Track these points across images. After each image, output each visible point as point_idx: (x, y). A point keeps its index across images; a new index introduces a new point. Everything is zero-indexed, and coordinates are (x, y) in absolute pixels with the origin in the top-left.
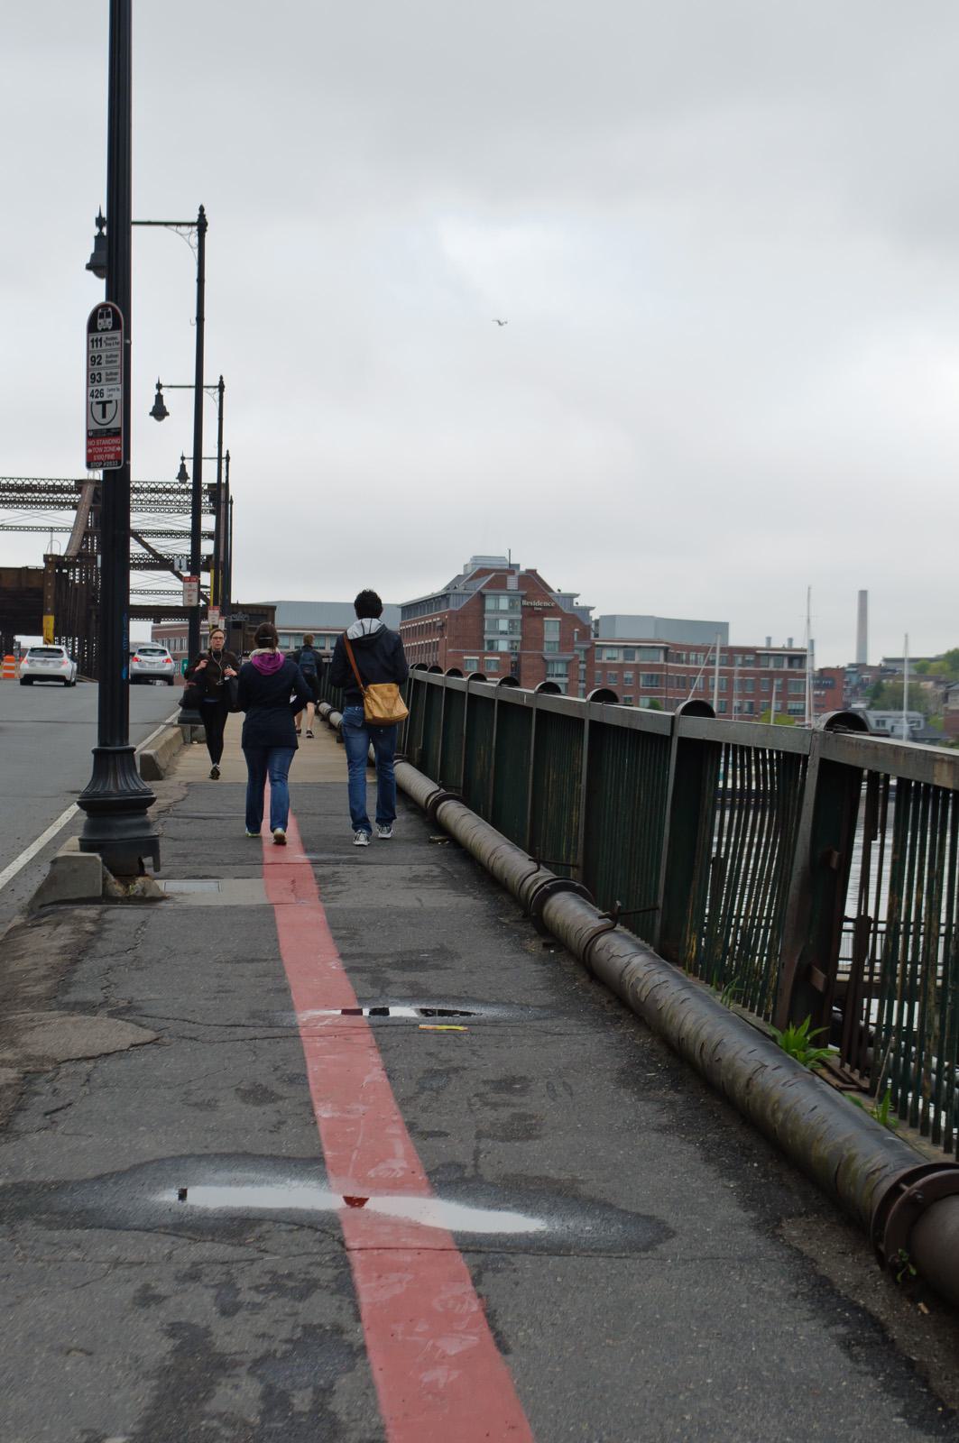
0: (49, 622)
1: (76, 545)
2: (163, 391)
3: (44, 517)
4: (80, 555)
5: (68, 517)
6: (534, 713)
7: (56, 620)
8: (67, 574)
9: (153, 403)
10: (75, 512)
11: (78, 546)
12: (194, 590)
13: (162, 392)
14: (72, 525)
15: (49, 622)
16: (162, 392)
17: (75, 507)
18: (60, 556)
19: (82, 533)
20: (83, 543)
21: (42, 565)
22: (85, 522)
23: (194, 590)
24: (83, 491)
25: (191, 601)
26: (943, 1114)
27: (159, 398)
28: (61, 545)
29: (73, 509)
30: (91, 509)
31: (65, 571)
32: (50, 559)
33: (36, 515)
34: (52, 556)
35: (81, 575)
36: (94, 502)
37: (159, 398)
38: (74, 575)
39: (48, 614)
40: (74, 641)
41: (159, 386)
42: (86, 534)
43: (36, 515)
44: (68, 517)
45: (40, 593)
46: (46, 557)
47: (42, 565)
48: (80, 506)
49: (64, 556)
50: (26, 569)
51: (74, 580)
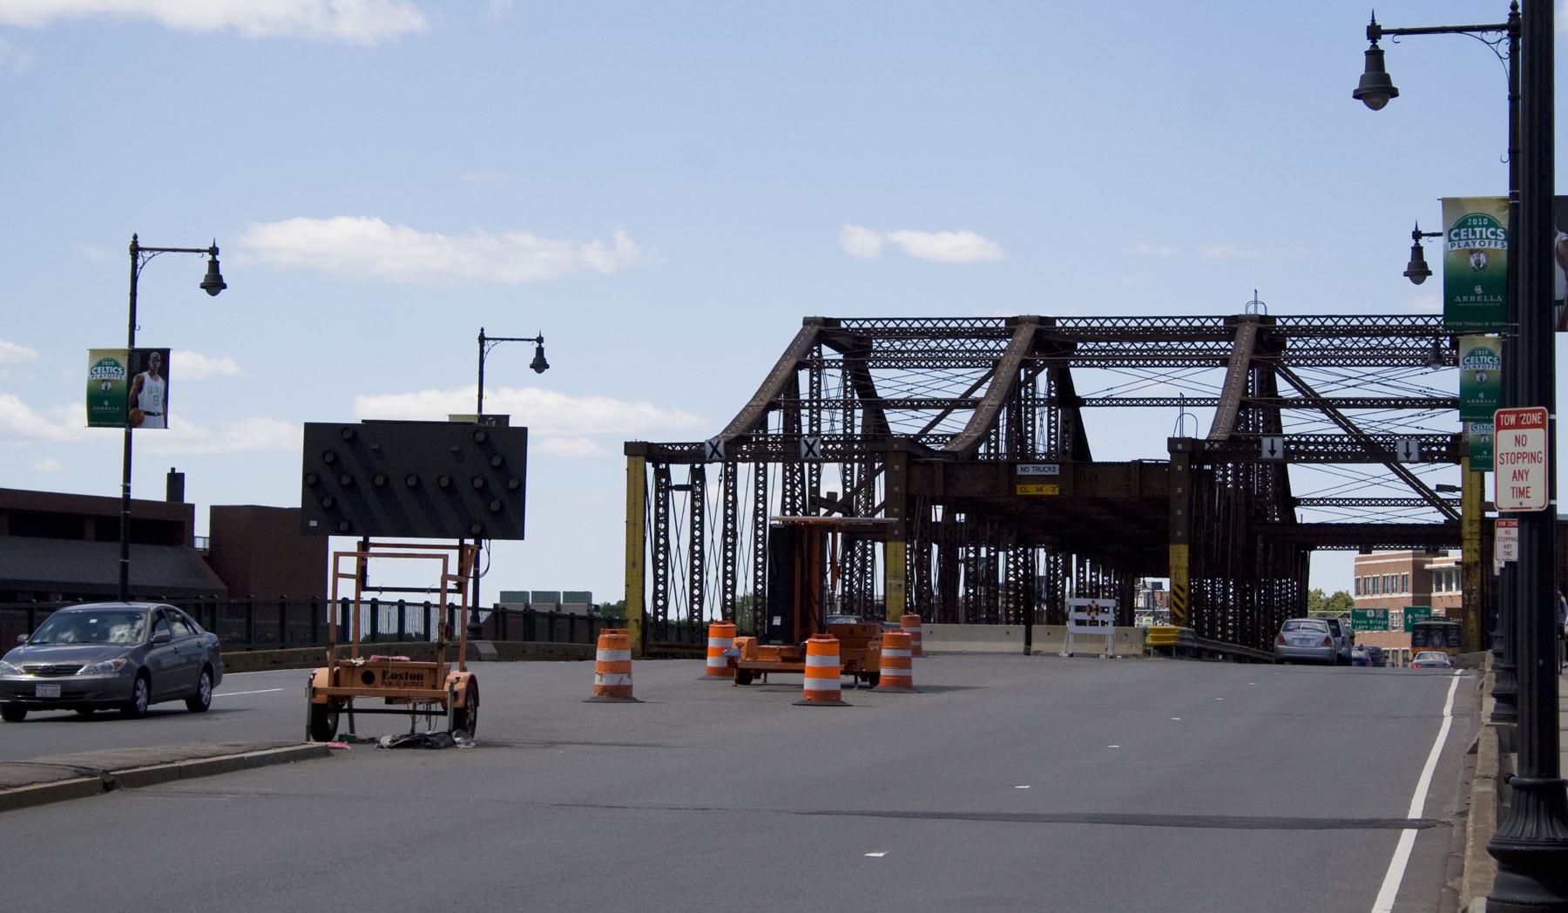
0: (1179, 555)
1: (1226, 425)
2: (1384, 43)
3: (1174, 382)
4: (1232, 440)
5: (1212, 380)
6: (1417, 595)
7: (1190, 551)
8: (1212, 472)
9: (1360, 68)
10: (1224, 370)
11: (1229, 426)
12: (1533, 457)
13: (1381, 44)
14: (1218, 393)
15: (1179, 555)
16: (1381, 44)
17: (1225, 362)
18: (1196, 441)
19: (1236, 403)
20: (1238, 421)
21: (1164, 455)
22: (1241, 384)
23: (1533, 457)
24: (1238, 335)
25: (1522, 492)
26: (1059, 410)
27: (1375, 58)
28: (1200, 424)
29: (1222, 365)
30: (1252, 365)
31: (1208, 467)
32: (1180, 446)
33: (1162, 379)
34: (1183, 440)
35: (1235, 475)
36: (1256, 351)
37: (1375, 58)
38: (1225, 475)
39: (1179, 542)
40: (1226, 587)
41: (1374, 32)
42: (1243, 405)
43: (1162, 379)
44: (1212, 380)
45: (1164, 504)
46: (1172, 443)
47: (1164, 455)
48: (1233, 361)
49: (1208, 440)
50: (1139, 464)
51: (1225, 482)
